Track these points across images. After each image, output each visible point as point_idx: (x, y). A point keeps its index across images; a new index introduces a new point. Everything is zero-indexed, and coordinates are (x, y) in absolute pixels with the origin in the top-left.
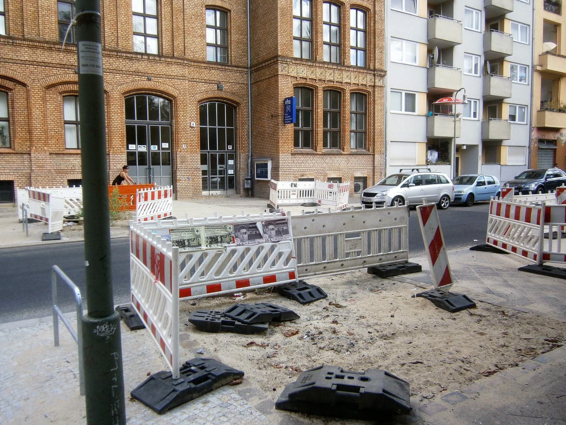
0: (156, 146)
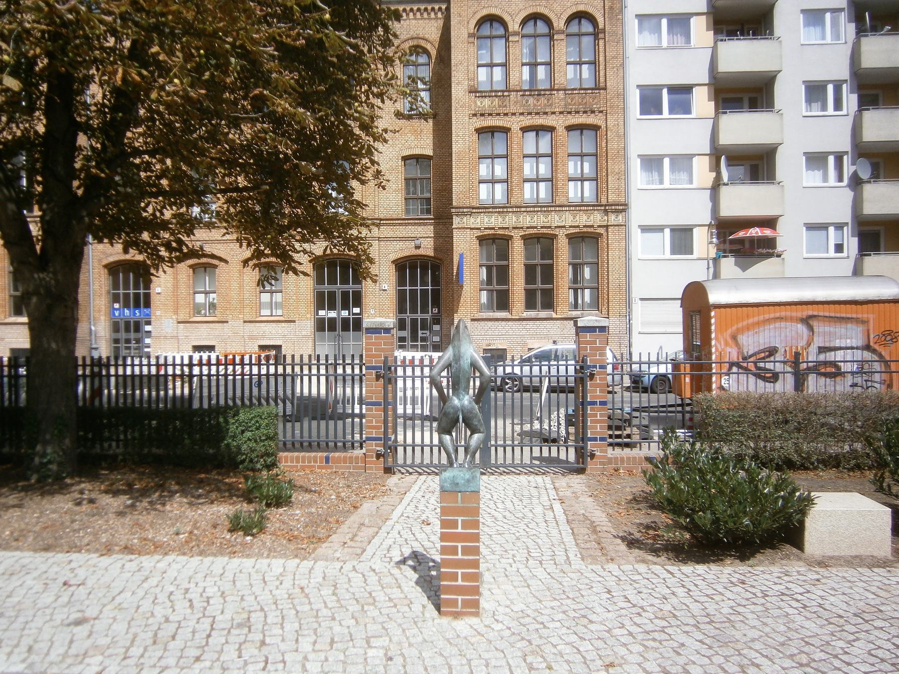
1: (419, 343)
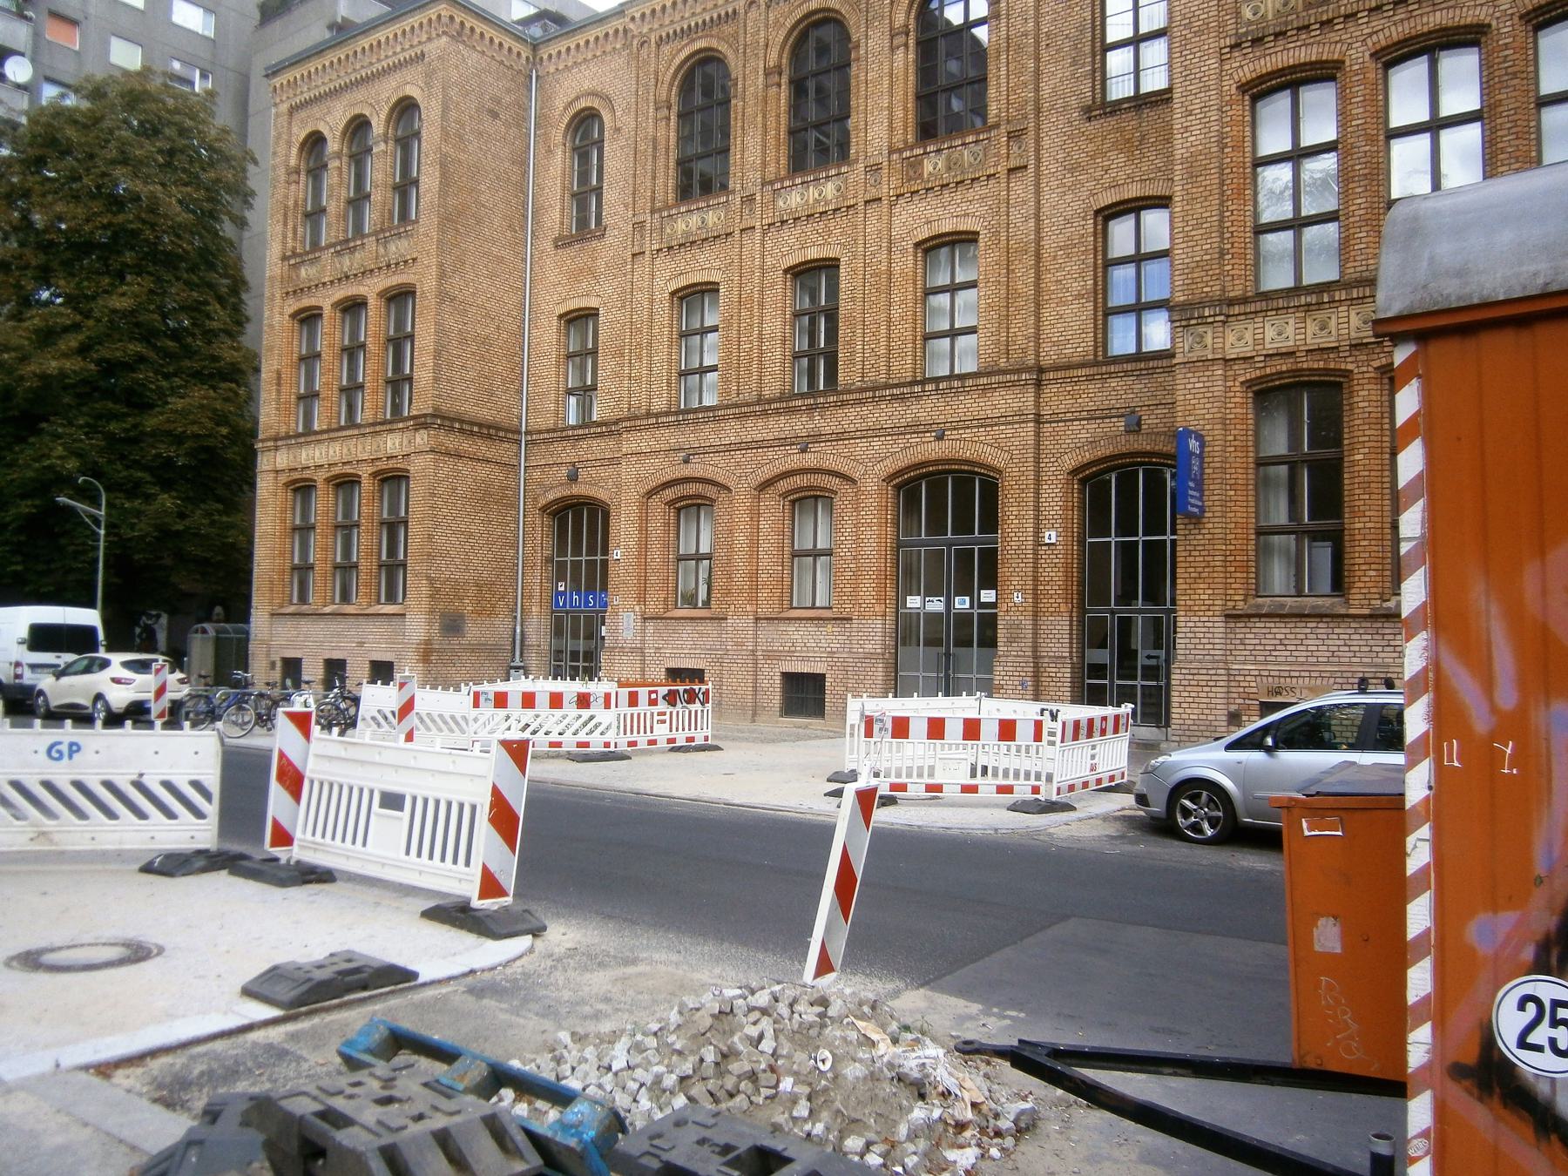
0: (967, 599)
1: (1139, 683)
